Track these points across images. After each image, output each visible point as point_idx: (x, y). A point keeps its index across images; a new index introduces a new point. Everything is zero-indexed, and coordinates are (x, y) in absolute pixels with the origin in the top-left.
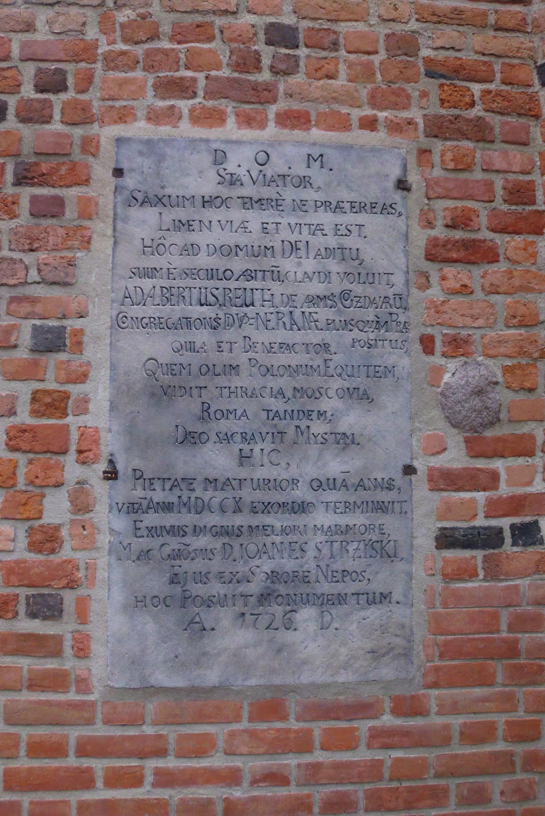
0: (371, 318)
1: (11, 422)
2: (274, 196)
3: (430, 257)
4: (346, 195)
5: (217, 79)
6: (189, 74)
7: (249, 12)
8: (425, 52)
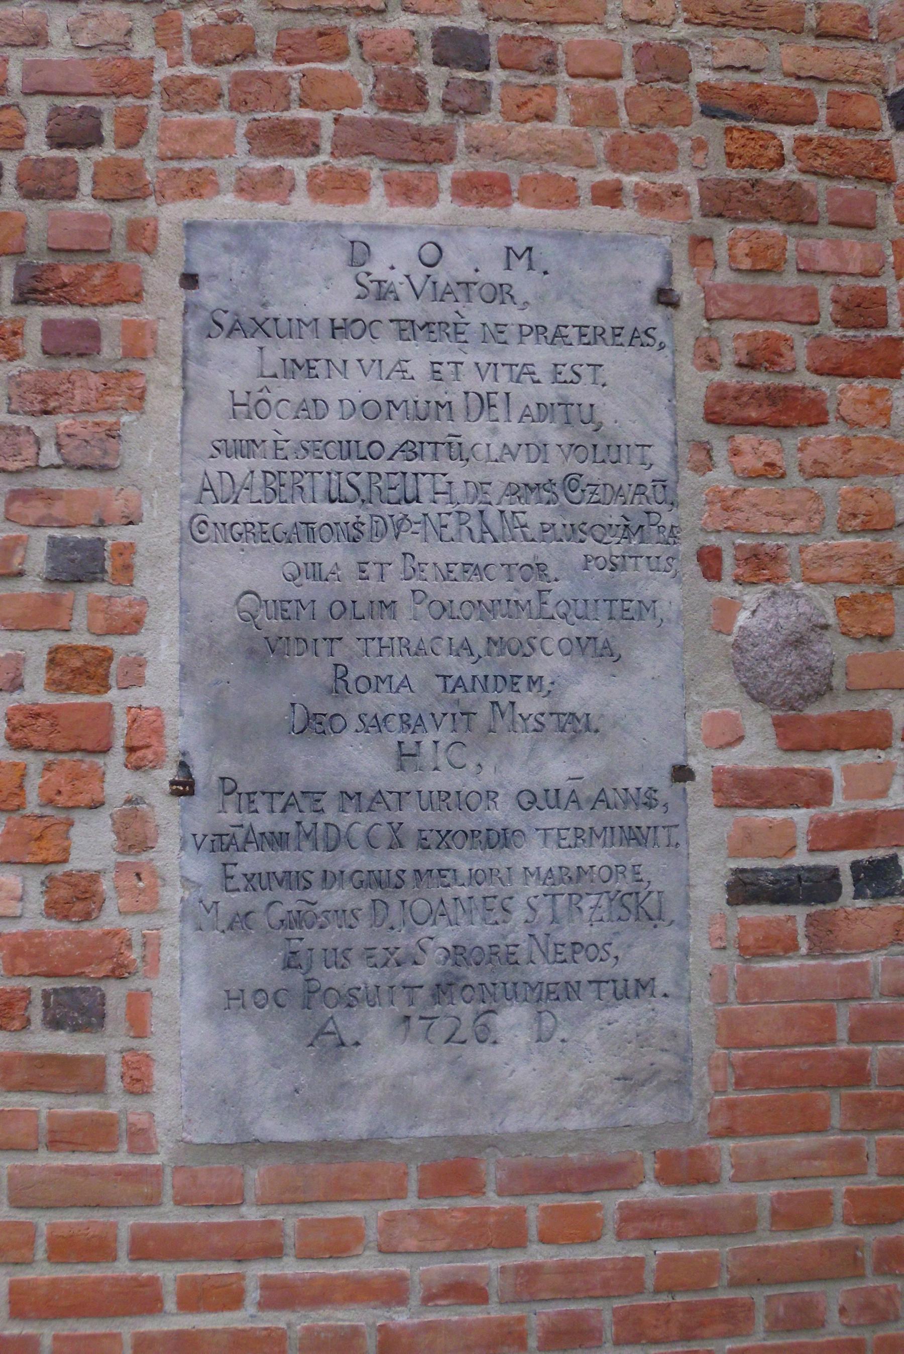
0: (616, 520)
1: (15, 701)
2: (451, 318)
3: (713, 418)
4: (570, 315)
5: (353, 122)
6: (306, 114)
8: (700, 75)
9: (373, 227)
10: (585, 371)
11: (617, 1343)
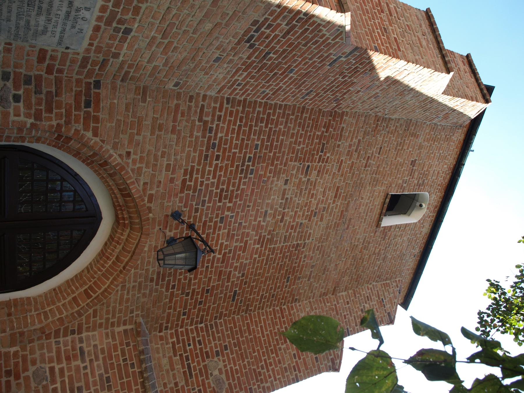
0: (20, 33)
1: (150, 251)
2: (69, 19)
3: (41, 50)
4: (66, 36)
5: (117, 14)
6: (122, 7)
7: (168, 8)
8: (111, 60)
9: (93, 12)
10: (54, 35)
11: (101, 391)
